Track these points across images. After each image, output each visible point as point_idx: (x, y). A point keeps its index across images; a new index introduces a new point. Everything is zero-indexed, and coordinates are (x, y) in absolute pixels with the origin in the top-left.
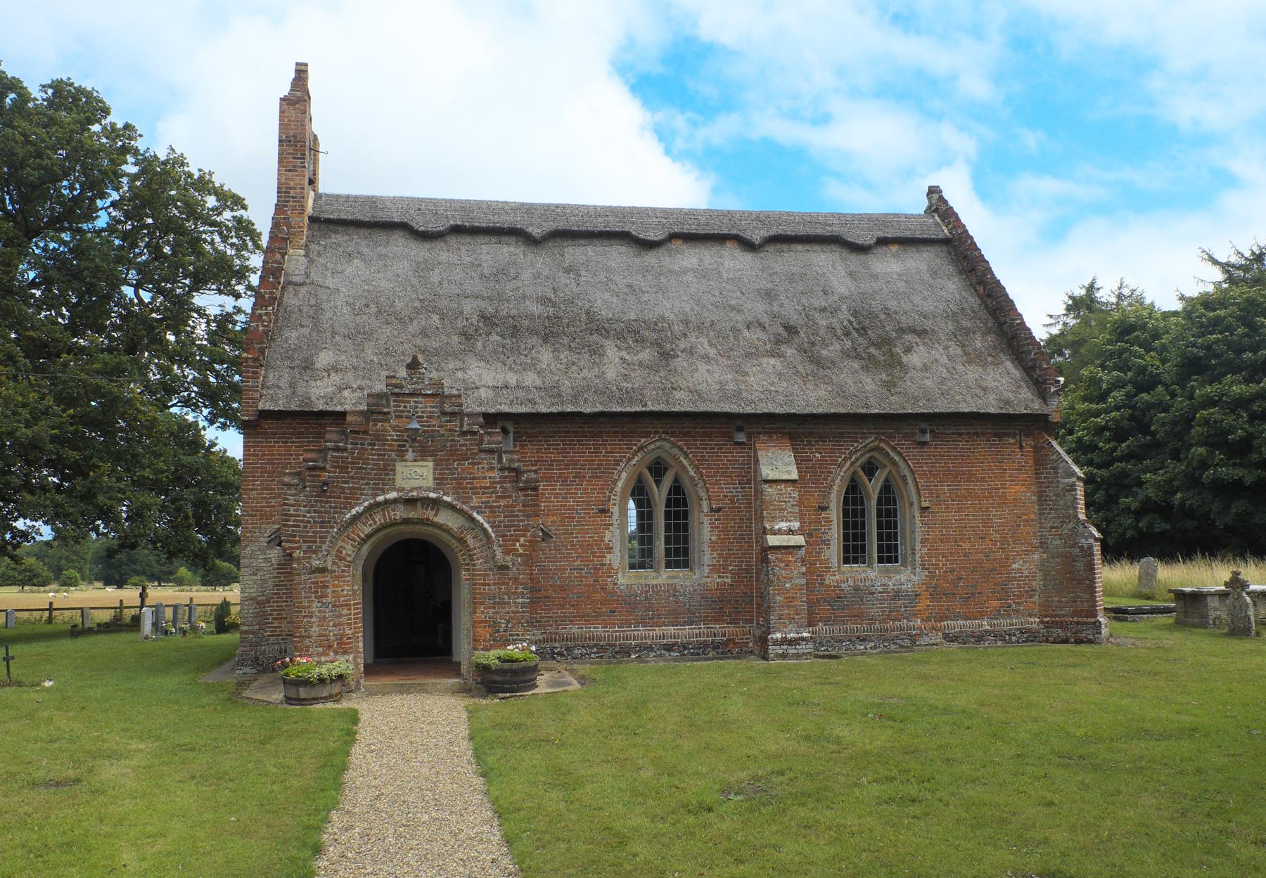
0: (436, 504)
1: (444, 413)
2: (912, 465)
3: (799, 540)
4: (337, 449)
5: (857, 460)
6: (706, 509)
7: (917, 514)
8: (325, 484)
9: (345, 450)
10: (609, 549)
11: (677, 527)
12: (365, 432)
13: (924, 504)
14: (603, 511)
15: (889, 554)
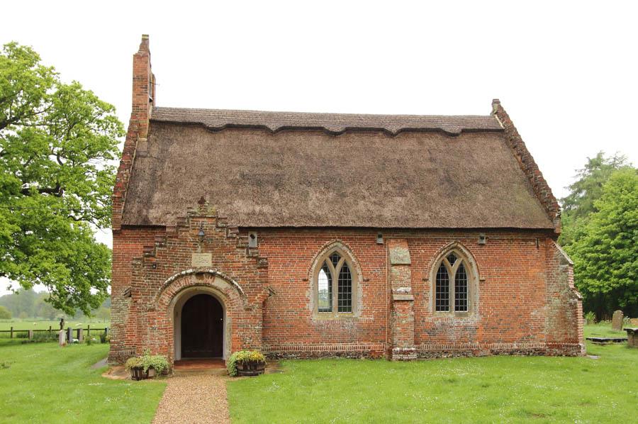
0: (213, 275)
2: (472, 258)
3: (411, 297)
5: (444, 254)
10: (364, 299)
11: (345, 296)
13: (481, 279)
14: (305, 280)
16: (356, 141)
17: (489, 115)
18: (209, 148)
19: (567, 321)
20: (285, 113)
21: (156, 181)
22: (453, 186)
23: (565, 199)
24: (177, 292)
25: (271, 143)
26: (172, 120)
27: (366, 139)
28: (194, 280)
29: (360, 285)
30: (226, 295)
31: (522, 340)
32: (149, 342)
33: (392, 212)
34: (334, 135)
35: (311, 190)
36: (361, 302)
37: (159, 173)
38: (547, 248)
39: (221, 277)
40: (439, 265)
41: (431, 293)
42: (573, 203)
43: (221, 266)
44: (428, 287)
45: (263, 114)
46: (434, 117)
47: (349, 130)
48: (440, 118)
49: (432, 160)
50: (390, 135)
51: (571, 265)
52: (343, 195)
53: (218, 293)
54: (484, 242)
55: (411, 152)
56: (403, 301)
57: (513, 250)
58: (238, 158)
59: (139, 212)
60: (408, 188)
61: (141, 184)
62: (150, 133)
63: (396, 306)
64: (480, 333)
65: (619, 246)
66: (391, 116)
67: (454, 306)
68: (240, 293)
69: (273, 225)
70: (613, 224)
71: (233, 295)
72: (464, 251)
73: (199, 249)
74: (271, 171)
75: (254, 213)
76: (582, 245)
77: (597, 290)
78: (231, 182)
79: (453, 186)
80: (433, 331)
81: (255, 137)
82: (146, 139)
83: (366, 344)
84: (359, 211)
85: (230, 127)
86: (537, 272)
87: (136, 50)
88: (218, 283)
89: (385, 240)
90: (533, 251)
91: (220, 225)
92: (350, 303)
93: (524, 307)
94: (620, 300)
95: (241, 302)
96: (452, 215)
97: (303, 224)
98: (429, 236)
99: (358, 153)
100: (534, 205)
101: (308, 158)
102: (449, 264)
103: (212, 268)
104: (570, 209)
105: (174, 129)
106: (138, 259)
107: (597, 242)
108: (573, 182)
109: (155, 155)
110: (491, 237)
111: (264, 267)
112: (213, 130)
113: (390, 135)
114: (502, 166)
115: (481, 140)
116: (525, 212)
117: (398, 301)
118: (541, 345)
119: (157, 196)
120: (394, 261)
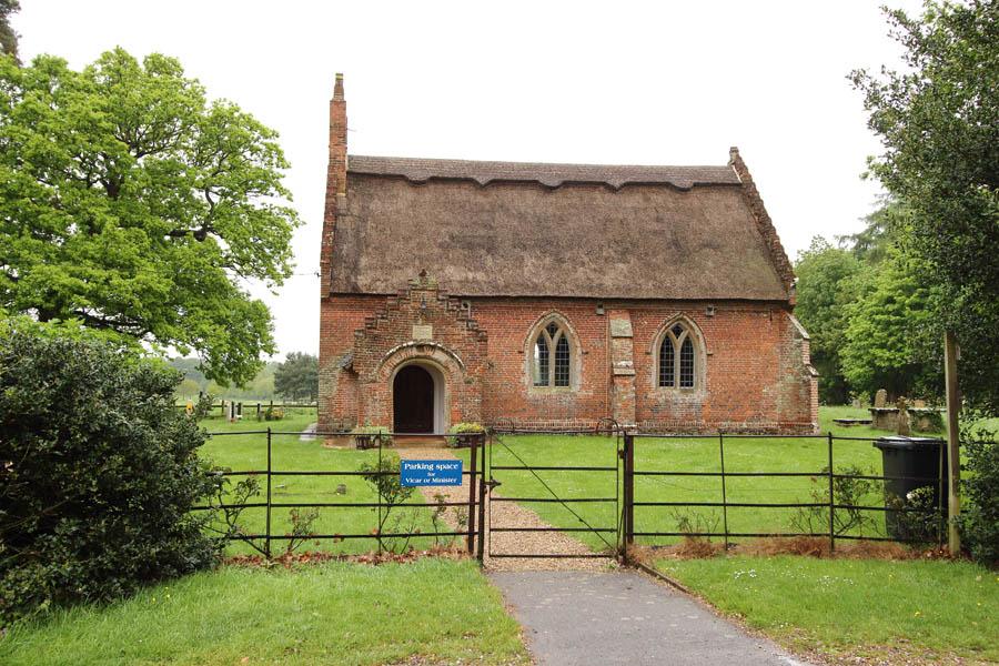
0: (433, 347)
2: (698, 330)
3: (633, 372)
10: (583, 373)
14: (520, 352)
16: (574, 196)
17: (726, 165)
18: (413, 205)
19: (799, 397)
20: (495, 163)
21: (361, 244)
22: (680, 251)
23: (858, 236)
24: (398, 364)
25: (480, 199)
26: (372, 172)
27: (586, 194)
28: (415, 352)
29: (577, 358)
30: (446, 368)
31: (752, 419)
33: (614, 279)
34: (550, 189)
35: (525, 254)
36: (580, 377)
37: (363, 235)
38: (781, 321)
39: (442, 350)
40: (663, 336)
41: (655, 369)
42: (869, 242)
43: (441, 338)
44: (651, 360)
45: (470, 164)
46: (662, 168)
47: (566, 184)
48: (669, 169)
49: (658, 220)
50: (612, 189)
51: (805, 339)
52: (561, 261)
53: (438, 366)
54: (712, 313)
55: (636, 210)
56: (624, 376)
57: (744, 323)
58: (446, 216)
59: (348, 278)
60: (633, 253)
61: (345, 247)
62: (349, 186)
63: (617, 381)
64: (706, 411)
65: (915, 306)
66: (614, 167)
68: (460, 366)
69: (488, 294)
70: (909, 277)
71: (453, 367)
72: (691, 323)
73: (420, 322)
74: (482, 232)
75: (467, 280)
76: (870, 304)
77: (887, 364)
78: (441, 246)
79: (680, 251)
80: (655, 408)
81: (463, 192)
82: (344, 195)
83: (584, 421)
84: (577, 280)
85: (434, 180)
86: (769, 346)
87: (331, 96)
88: (438, 355)
89: (606, 310)
90: (766, 323)
91: (440, 297)
93: (756, 384)
94: (916, 378)
95: (461, 375)
96: (678, 284)
97: (520, 294)
98: (652, 307)
99: (577, 211)
100: (768, 273)
101: (522, 217)
103: (433, 341)
104: (865, 249)
105: (374, 182)
106: (359, 331)
107: (890, 300)
108: (871, 211)
109: (356, 213)
110: (720, 308)
111: (484, 340)
112: (416, 184)
113: (612, 189)
114: (737, 227)
115: (715, 196)
116: (755, 279)
117: (619, 375)
118: (773, 425)
119: (364, 261)
120: (614, 334)
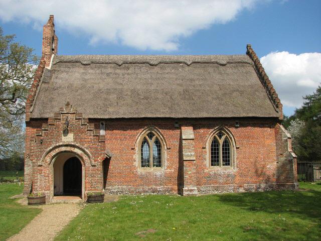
0: (74, 146)
1: (76, 119)
2: (235, 133)
3: (194, 159)
4: (45, 130)
5: (215, 132)
6: (166, 148)
7: (235, 149)
8: (42, 140)
9: (47, 130)
10: (135, 161)
11: (226, 157)
12: (54, 125)
13: (237, 147)
14: (133, 149)
15: (227, 162)
32: (39, 183)
67: (222, 163)
92: (229, 161)
102: (218, 138)
